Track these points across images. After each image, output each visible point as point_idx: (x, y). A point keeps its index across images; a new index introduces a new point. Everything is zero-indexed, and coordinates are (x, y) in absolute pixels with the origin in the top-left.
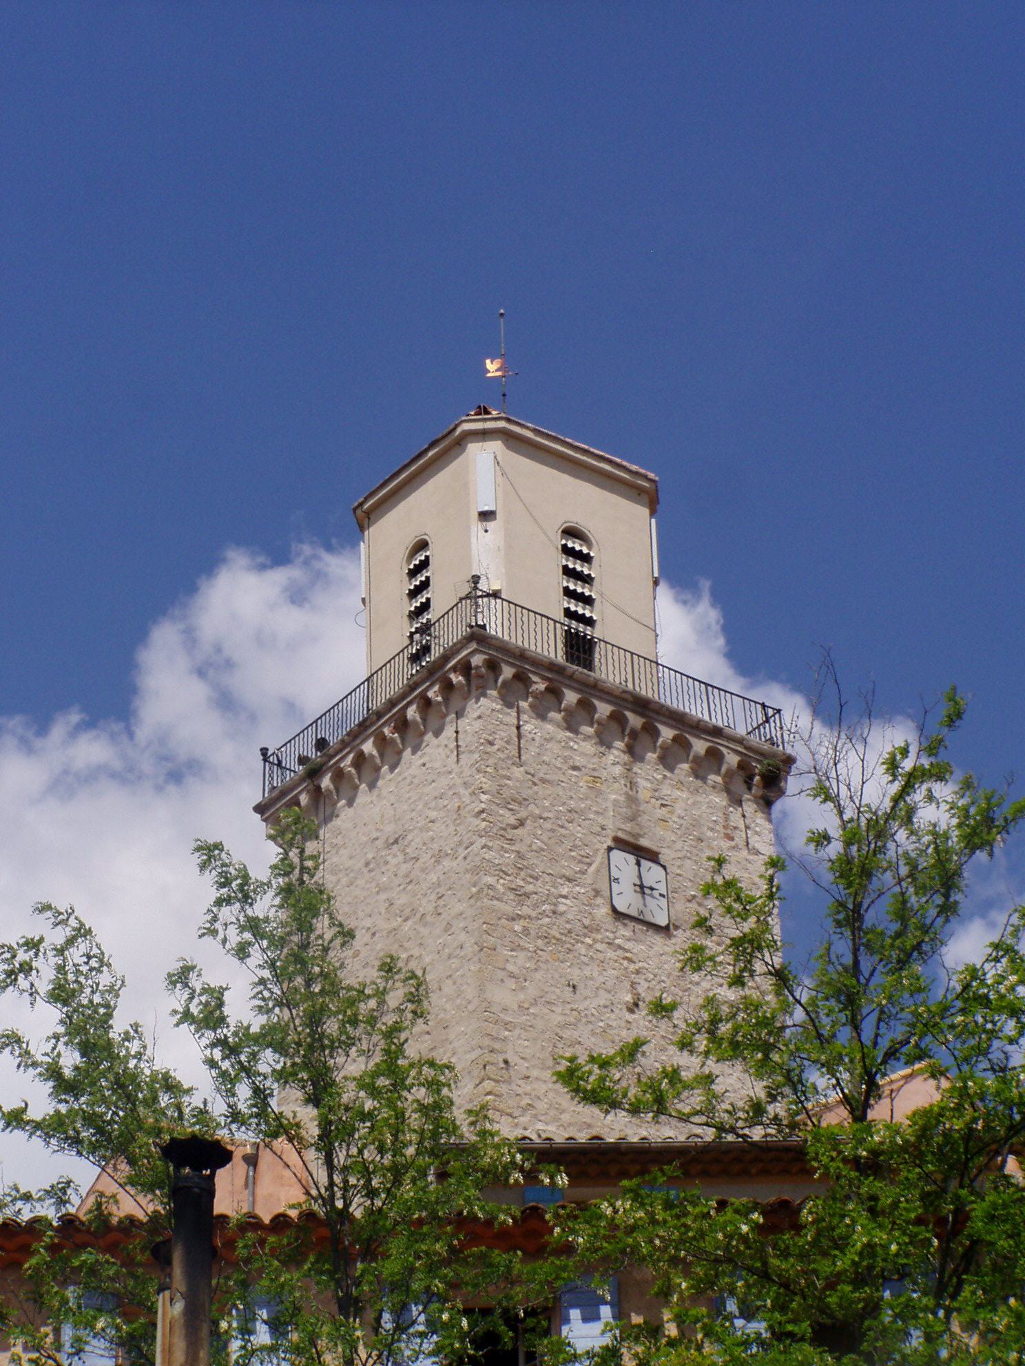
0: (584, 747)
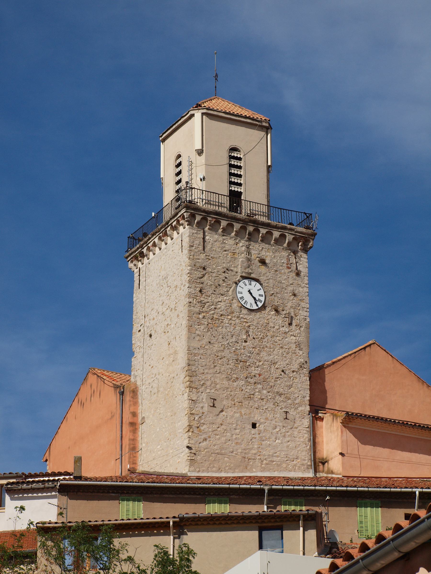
0: (230, 242)
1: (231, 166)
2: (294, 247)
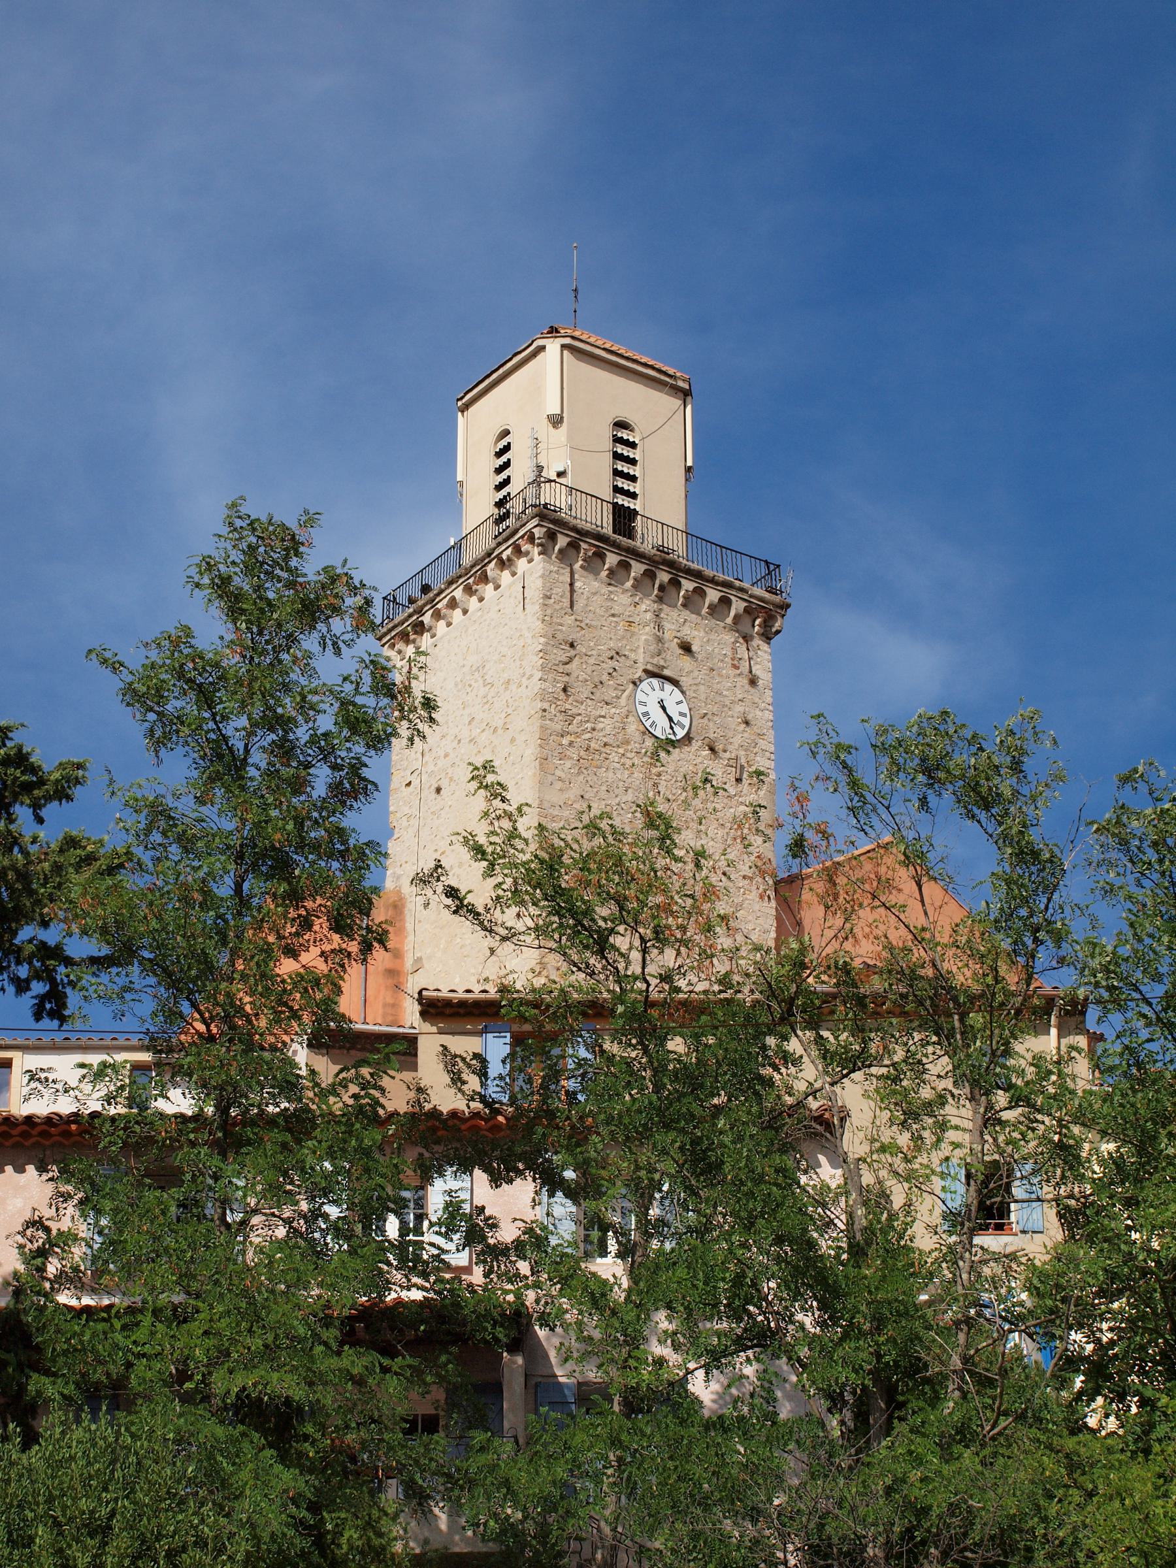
0: (622, 598)
1: (617, 456)
2: (745, 626)
